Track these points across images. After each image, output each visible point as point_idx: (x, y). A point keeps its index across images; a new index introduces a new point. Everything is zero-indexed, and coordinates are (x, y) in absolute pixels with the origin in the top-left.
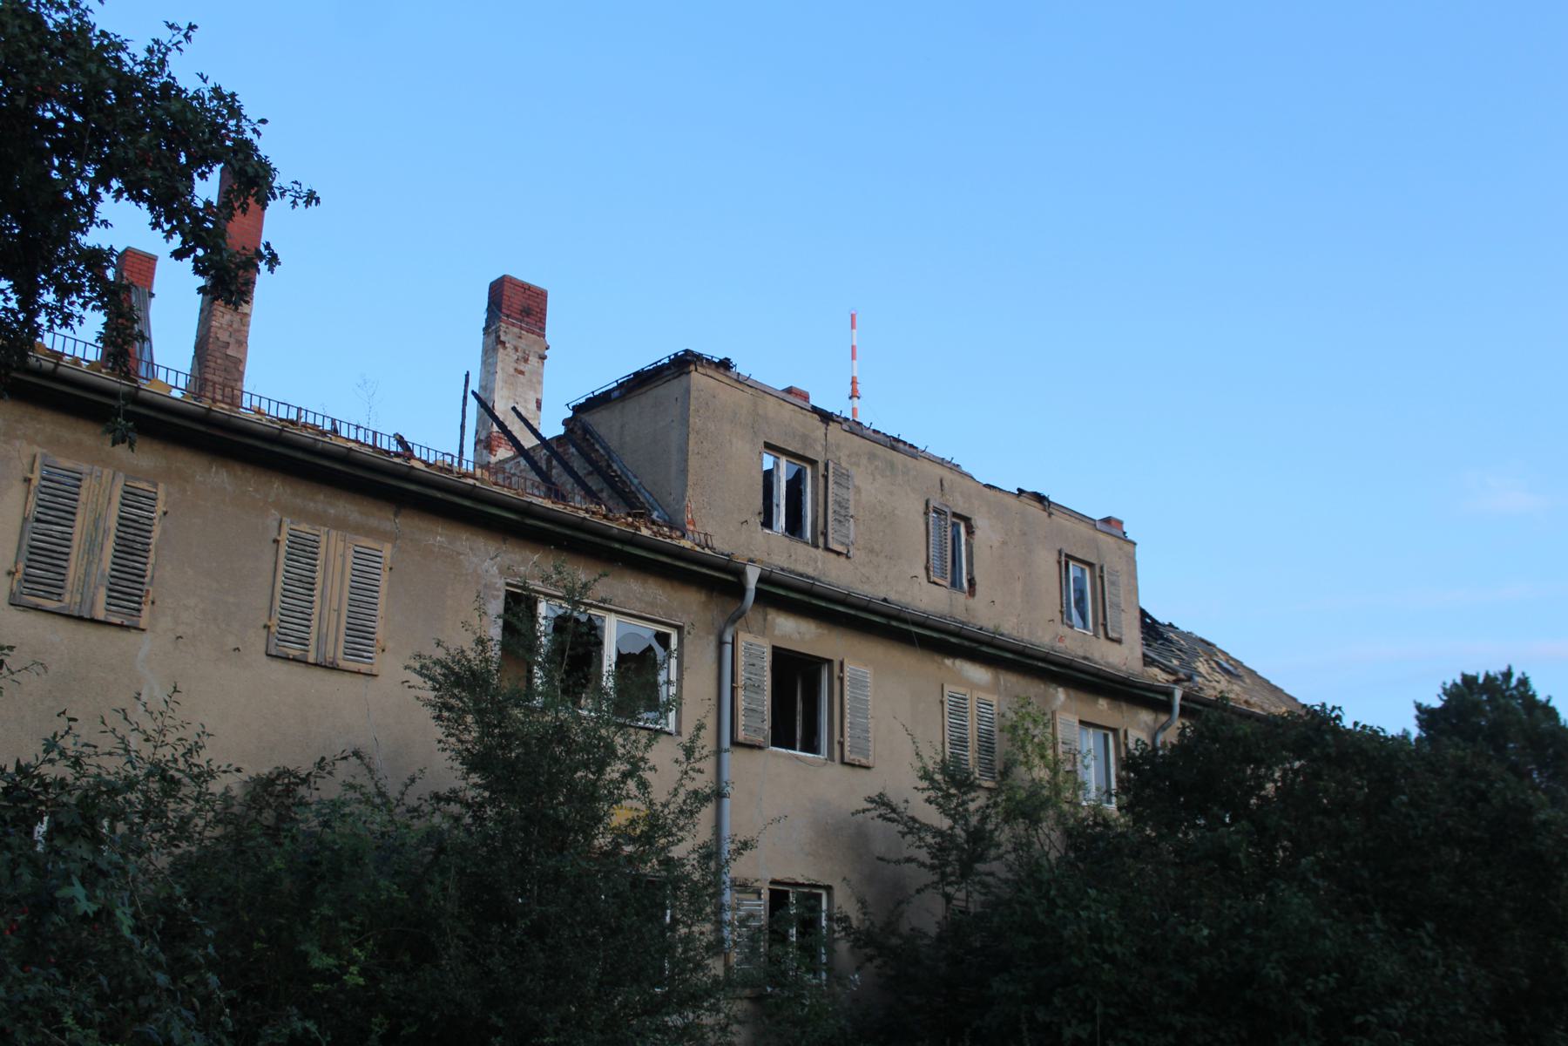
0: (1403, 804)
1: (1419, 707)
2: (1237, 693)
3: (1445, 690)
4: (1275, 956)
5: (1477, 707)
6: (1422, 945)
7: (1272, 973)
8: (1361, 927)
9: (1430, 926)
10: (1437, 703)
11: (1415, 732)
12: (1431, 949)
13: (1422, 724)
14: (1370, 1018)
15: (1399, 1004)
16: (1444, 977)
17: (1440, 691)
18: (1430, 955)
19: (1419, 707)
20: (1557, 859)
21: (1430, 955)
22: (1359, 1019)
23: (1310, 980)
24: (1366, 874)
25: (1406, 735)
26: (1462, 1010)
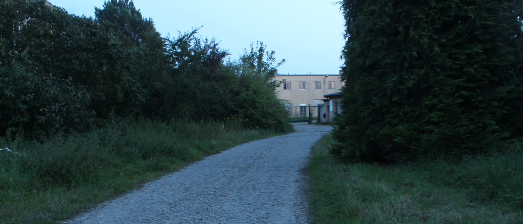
0: (64, 35)
1: (96, 9)
2: (50, 5)
3: (105, 3)
4: (10, 87)
5: (115, 10)
6: (68, 84)
7: (9, 94)
8: (44, 78)
9: (71, 78)
10: (102, 8)
11: (94, 18)
12: (71, 86)
13: (97, 15)
14: (45, 109)
15: (57, 104)
16: (74, 96)
17: (104, 4)
18: (70, 88)
19: (96, 9)
20: (116, 57)
21: (70, 88)
22: (41, 110)
23: (23, 96)
24: (50, 59)
25: (90, 19)
26: (78, 106)
